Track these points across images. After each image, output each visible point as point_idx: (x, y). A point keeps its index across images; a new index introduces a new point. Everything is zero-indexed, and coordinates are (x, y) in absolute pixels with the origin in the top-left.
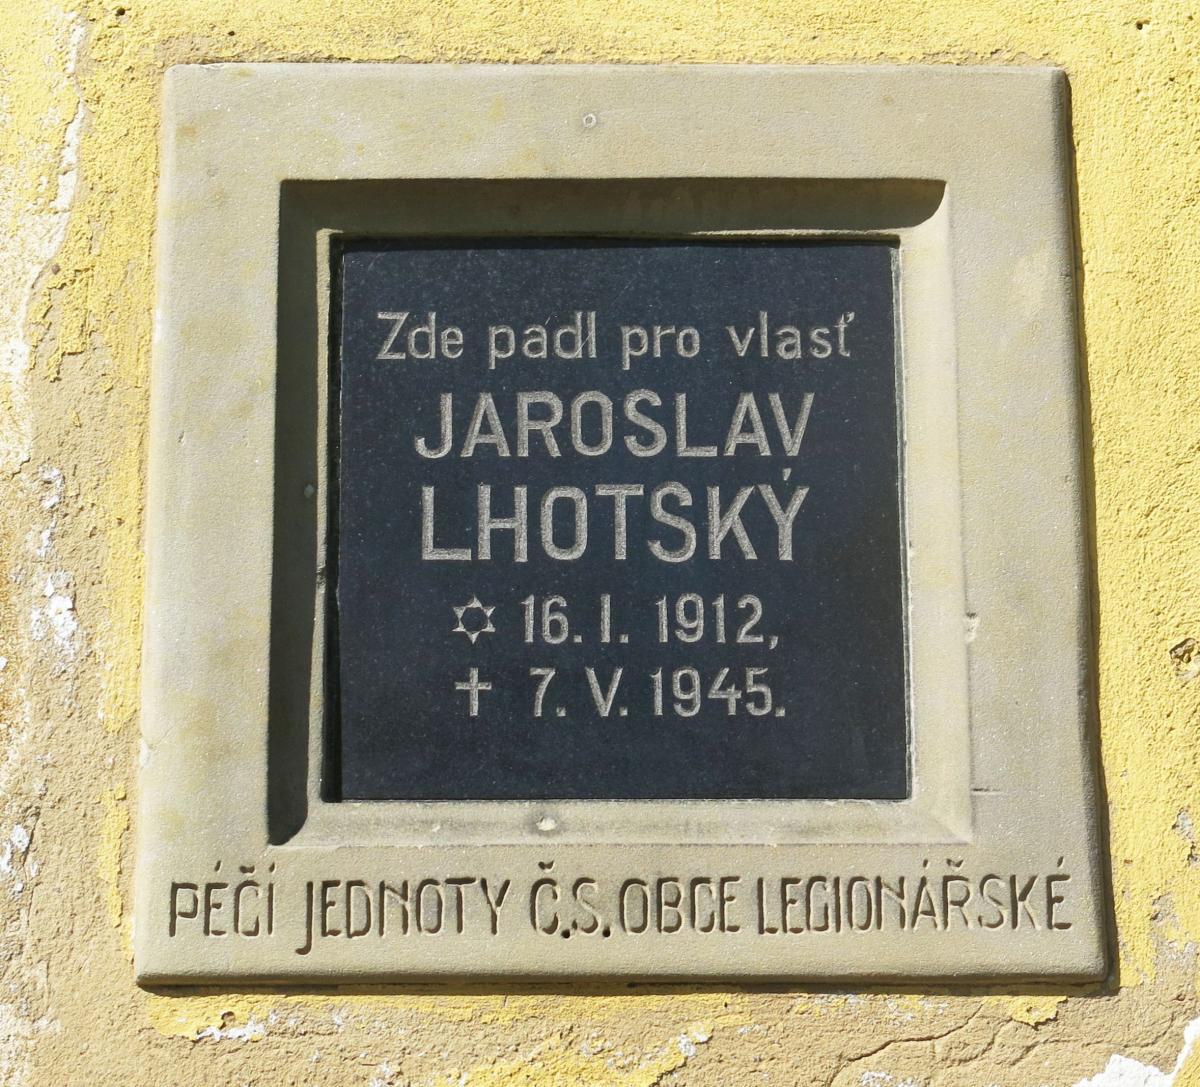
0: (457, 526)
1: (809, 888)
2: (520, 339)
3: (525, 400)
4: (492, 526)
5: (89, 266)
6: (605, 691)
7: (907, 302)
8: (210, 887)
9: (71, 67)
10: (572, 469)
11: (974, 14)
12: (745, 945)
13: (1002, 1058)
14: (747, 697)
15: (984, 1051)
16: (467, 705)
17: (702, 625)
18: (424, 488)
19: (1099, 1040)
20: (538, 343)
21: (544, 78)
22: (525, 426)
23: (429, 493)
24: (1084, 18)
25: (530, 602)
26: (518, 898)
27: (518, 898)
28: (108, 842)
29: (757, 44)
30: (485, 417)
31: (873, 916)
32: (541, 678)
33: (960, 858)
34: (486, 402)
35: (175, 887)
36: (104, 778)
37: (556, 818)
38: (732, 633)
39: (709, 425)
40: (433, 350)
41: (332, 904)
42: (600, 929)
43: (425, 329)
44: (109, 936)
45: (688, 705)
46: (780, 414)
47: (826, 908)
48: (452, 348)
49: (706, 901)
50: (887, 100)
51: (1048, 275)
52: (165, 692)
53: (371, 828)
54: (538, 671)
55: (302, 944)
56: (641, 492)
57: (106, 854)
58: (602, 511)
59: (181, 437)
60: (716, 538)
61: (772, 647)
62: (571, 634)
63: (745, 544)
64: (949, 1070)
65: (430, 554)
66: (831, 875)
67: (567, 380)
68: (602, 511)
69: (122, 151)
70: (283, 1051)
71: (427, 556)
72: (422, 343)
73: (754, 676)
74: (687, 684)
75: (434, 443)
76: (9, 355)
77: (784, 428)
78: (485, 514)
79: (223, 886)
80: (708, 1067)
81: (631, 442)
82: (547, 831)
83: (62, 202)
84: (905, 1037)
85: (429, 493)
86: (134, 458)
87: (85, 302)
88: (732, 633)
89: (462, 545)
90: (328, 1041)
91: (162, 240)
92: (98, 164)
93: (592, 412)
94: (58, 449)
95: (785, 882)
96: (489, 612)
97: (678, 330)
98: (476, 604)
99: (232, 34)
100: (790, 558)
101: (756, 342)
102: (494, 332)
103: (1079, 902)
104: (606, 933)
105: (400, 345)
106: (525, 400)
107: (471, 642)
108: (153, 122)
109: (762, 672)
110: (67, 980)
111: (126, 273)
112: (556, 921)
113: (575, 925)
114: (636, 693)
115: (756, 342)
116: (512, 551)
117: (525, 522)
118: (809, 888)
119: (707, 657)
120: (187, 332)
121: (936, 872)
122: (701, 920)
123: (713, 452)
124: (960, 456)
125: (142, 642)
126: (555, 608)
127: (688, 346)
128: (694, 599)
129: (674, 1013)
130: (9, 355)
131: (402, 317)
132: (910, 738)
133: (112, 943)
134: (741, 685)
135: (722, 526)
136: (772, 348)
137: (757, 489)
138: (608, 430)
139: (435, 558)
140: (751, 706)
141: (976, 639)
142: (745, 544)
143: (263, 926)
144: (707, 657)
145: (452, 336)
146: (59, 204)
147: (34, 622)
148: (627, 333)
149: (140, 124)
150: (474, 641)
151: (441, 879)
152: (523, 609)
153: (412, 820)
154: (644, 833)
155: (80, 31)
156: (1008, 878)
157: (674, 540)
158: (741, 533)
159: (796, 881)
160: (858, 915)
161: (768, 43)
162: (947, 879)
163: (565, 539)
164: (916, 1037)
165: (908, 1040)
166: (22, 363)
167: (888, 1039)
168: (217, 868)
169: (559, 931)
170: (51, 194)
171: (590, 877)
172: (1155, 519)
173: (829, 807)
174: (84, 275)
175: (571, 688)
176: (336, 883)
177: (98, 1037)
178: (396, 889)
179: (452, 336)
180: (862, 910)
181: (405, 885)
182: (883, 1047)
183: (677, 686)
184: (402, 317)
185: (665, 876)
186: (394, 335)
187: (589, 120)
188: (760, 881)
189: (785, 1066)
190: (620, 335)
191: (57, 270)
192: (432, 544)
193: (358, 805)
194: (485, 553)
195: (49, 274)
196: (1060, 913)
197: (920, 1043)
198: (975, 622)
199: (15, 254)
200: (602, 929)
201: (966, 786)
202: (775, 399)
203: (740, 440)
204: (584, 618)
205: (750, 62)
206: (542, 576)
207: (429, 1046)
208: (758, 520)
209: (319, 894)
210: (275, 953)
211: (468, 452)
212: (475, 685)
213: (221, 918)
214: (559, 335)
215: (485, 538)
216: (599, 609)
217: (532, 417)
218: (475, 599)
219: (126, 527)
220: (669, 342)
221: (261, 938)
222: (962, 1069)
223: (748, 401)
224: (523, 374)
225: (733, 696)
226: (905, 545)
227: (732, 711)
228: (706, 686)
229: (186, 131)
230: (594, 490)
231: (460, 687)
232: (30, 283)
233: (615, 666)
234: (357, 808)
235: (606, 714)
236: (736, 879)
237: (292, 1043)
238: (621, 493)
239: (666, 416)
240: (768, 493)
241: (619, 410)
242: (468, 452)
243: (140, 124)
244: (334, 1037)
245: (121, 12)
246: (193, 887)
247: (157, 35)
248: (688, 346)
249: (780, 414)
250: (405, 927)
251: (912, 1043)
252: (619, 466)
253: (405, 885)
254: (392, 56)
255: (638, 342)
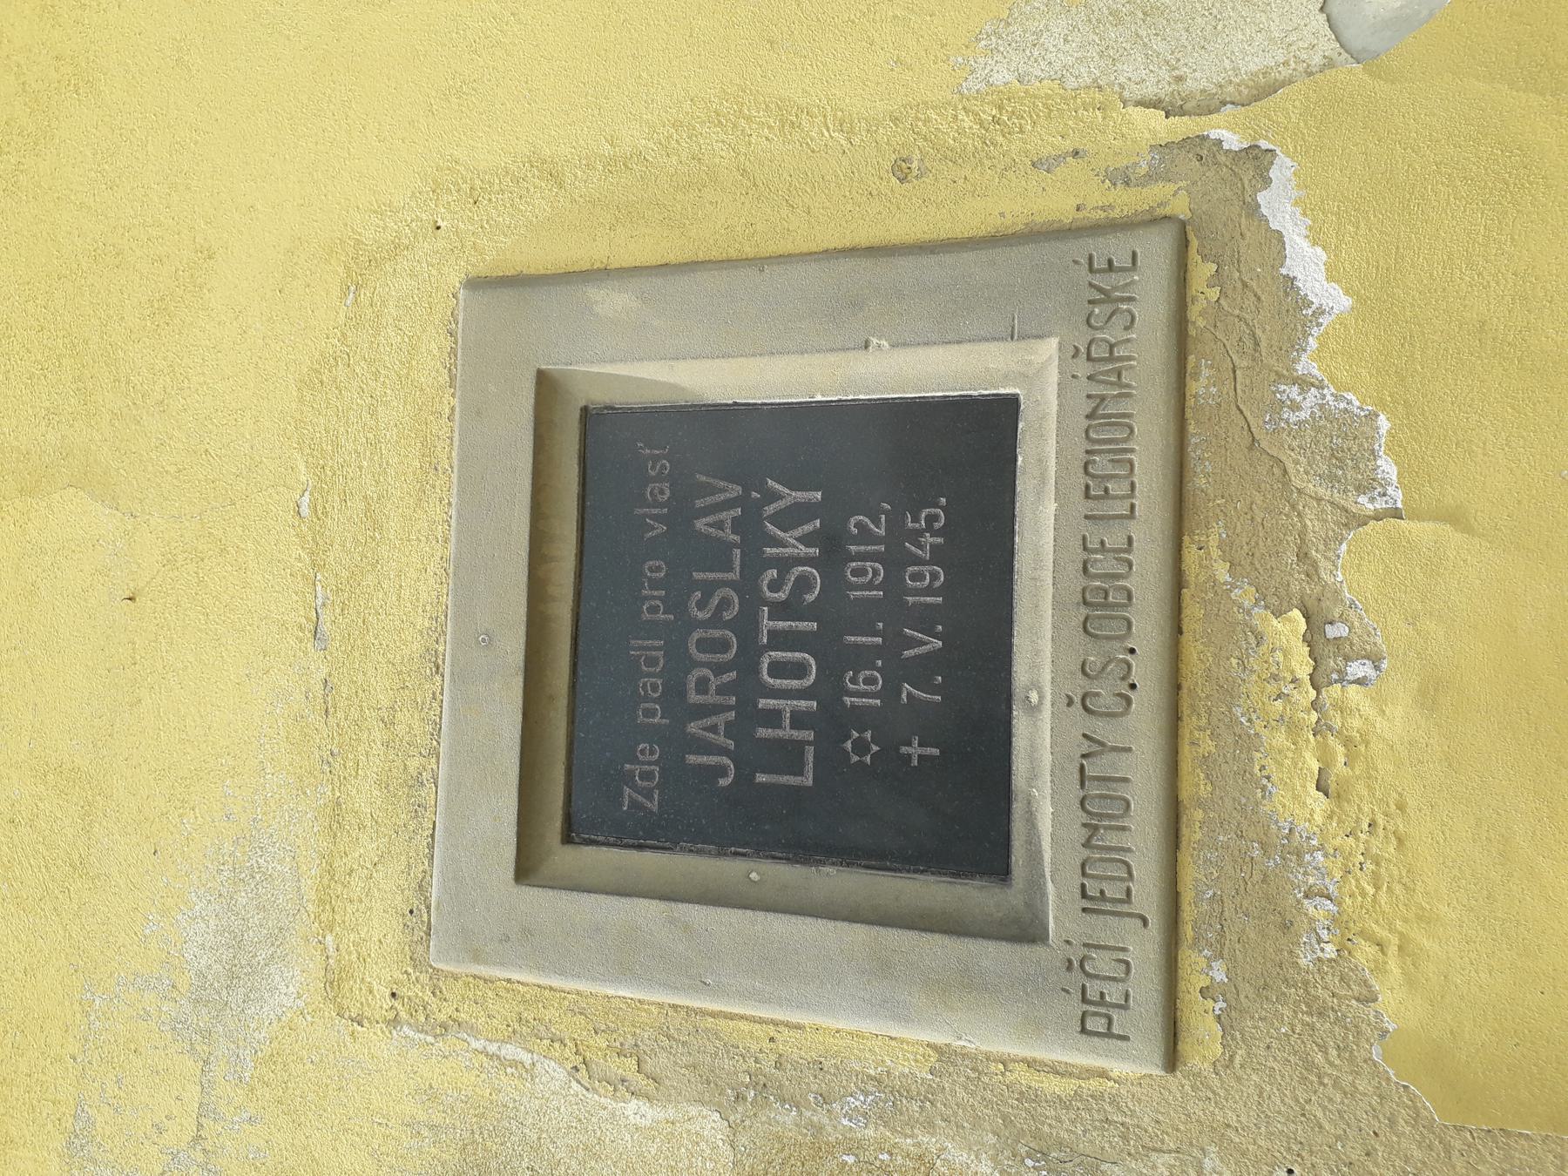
0: (789, 756)
1: (1093, 476)
2: (646, 699)
3: (694, 698)
4: (788, 728)
5: (574, 1042)
6: (923, 643)
7: (630, 401)
8: (1084, 1000)
9: (430, 1039)
10: (747, 663)
11: (424, 351)
12: (1145, 532)
13: (1253, 309)
14: (929, 528)
15: (1248, 325)
16: (931, 758)
17: (869, 563)
18: (757, 781)
19: (1237, 225)
20: (651, 683)
21: (452, 674)
22: (711, 698)
23: (761, 778)
24: (430, 268)
25: (848, 700)
26: (1100, 728)
27: (1100, 728)
28: (1042, 1082)
29: (438, 512)
30: (704, 729)
31: (1123, 422)
32: (909, 694)
33: (1072, 348)
34: (693, 728)
35: (1083, 1030)
36: (986, 1080)
37: (1028, 689)
38: (876, 540)
39: (718, 556)
40: (653, 767)
41: (1102, 892)
42: (1129, 657)
43: (637, 772)
44: (1128, 1092)
45: (934, 576)
46: (709, 500)
47: (1112, 460)
48: (652, 753)
49: (1102, 564)
50: (478, 413)
51: (608, 289)
52: (913, 1021)
53: (1033, 849)
54: (904, 696)
55: (1139, 923)
56: (766, 608)
57: (1054, 1086)
58: (780, 640)
59: (705, 984)
60: (803, 550)
61: (889, 507)
62: (875, 668)
63: (808, 528)
64: (1263, 354)
65: (808, 780)
66: (1083, 457)
67: (679, 662)
68: (780, 640)
69: (491, 1006)
70: (1237, 946)
71: (810, 782)
72: (646, 776)
73: (912, 522)
74: (917, 577)
75: (723, 771)
76: (638, 1117)
77: (722, 497)
78: (780, 733)
79: (1084, 988)
80: (1258, 566)
81: (727, 616)
82: (1039, 697)
83: (526, 1058)
84: (1232, 393)
85: (761, 778)
86: (722, 1022)
87: (600, 1049)
88: (876, 540)
89: (802, 754)
90: (1228, 903)
91: (556, 982)
92: (500, 1026)
93: (703, 645)
94: (712, 1085)
95: (1087, 496)
96: (855, 734)
97: (646, 576)
98: (849, 745)
99: (411, 912)
100: (820, 493)
101: (655, 518)
102: (641, 719)
103: (1116, 248)
104: (1132, 651)
105: (648, 795)
106: (694, 698)
107: (879, 751)
108: (471, 979)
109: (909, 516)
110: (1167, 1134)
111: (581, 1013)
112: (1120, 695)
113: (1123, 679)
114: (924, 616)
115: (655, 518)
116: (808, 713)
117: (786, 702)
118: (1093, 476)
119: (896, 561)
120: (625, 971)
121: (1083, 368)
122: (1122, 570)
123: (737, 552)
124: (742, 356)
125: (870, 1033)
126: (854, 681)
127: (658, 569)
128: (850, 570)
129: (1206, 595)
130: (638, 1117)
131: (627, 790)
132: (966, 396)
133: (1135, 1089)
134: (920, 533)
135: (794, 546)
136: (662, 505)
137: (765, 519)
138: (717, 633)
139: (811, 776)
140: (937, 525)
141: (886, 340)
142: (808, 528)
143: (1088, 905)
144: (896, 561)
145: (642, 752)
146: (528, 1063)
147: (851, 1124)
148: (646, 616)
149: (472, 990)
150: (878, 749)
151: (1082, 794)
152: (853, 706)
153: (1027, 812)
154: (1042, 615)
155: (405, 1028)
156: (1091, 306)
157: (803, 584)
158: (799, 532)
159: (1087, 487)
160: (1120, 435)
161: (438, 503)
162: (1089, 358)
163: (800, 670)
164: (1233, 383)
165: (1235, 390)
166: (644, 1107)
167: (1234, 408)
168: (1067, 992)
169: (1130, 693)
170: (520, 1066)
171: (1081, 663)
172: (796, 201)
173: (1023, 461)
174: (580, 1047)
175: (921, 671)
176: (1083, 886)
177: (1222, 1113)
178: (1090, 834)
179: (642, 752)
180: (1116, 430)
181: (1084, 825)
182: (1242, 412)
183: (861, 580)
184: (627, 790)
185: (1081, 600)
186: (640, 798)
187: (484, 640)
188: (1087, 517)
189: (1258, 498)
190: (647, 621)
191: (576, 1069)
192: (800, 778)
193: (1013, 858)
194: (809, 735)
195: (578, 1076)
196: (1120, 260)
197: (1238, 379)
198: (875, 341)
199: (563, 1101)
200: (1129, 655)
201: (1011, 345)
202: (699, 503)
203: (728, 531)
204: (861, 659)
205: (451, 517)
206: (829, 689)
207: (1235, 814)
208: (789, 518)
209: (1092, 903)
210: (1144, 948)
211: (731, 744)
212: (914, 750)
213: (1113, 994)
214: (644, 668)
215: (797, 734)
216: (856, 645)
217: (706, 692)
218: (845, 745)
219: (777, 1036)
220: (655, 585)
221: (1133, 959)
222: (1263, 344)
223: (700, 524)
224: (674, 693)
225: (929, 539)
226: (812, 402)
227: (940, 540)
228: (919, 561)
229: (477, 957)
230: (764, 646)
231: (915, 762)
232: (585, 1092)
233: (901, 634)
234: (1016, 860)
235: (940, 643)
236: (1084, 538)
237: (1232, 936)
238: (767, 624)
239: (709, 589)
240: (770, 509)
241: (705, 624)
242: (731, 744)
243: (472, 990)
244: (1225, 898)
245: (393, 995)
246: (1084, 1015)
247: (410, 970)
248: (658, 569)
249: (709, 500)
250: (1124, 829)
251: (1238, 387)
252: (746, 626)
253: (1084, 825)
254: (434, 789)
255: (653, 607)
